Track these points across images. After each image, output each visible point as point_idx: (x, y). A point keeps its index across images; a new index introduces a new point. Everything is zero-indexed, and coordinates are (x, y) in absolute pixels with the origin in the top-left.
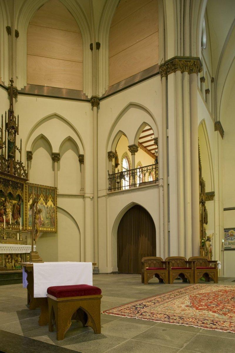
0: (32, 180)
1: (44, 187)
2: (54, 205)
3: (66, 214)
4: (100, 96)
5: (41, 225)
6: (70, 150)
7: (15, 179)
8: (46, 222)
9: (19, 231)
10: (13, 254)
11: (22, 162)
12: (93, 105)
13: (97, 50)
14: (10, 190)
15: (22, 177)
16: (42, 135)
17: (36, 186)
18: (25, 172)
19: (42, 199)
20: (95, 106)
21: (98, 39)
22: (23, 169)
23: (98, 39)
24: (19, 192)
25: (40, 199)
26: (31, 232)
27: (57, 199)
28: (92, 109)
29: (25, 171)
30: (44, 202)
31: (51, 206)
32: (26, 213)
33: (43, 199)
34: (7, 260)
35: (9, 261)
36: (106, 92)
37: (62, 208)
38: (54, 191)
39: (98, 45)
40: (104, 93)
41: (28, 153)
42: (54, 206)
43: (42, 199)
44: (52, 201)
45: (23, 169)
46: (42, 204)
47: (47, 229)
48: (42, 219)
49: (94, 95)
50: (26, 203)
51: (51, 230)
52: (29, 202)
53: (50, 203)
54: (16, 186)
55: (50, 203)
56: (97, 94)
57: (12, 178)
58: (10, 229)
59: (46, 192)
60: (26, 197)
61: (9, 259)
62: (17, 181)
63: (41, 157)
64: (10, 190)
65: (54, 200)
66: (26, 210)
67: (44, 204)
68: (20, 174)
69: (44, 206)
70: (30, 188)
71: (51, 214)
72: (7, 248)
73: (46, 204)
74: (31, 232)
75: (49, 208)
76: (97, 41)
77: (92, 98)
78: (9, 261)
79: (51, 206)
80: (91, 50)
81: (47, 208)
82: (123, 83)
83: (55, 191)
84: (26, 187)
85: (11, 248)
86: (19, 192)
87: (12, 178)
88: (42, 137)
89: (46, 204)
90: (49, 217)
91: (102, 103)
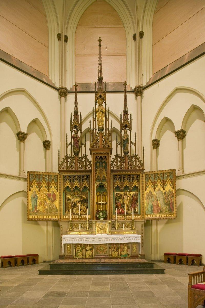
0: (148, 168)
1: (161, 172)
2: (173, 189)
3: (190, 195)
4: (144, 84)
5: (158, 212)
6: (168, 131)
7: (130, 172)
8: (164, 208)
9: (69, 221)
10: (119, 243)
11: (137, 154)
12: (137, 95)
13: (141, 39)
14: (126, 183)
15: (138, 168)
16: (165, 118)
17: (152, 173)
18: (140, 163)
19: (159, 185)
20: (139, 95)
21: (142, 28)
22: (139, 160)
23: (142, 28)
24: (135, 183)
25: (157, 185)
26: (157, 220)
27: (176, 181)
28: (136, 99)
29: (140, 162)
30: (161, 187)
31: (170, 190)
32: (143, 202)
33: (161, 185)
34: (113, 249)
35: (114, 250)
36: (150, 80)
37: (185, 189)
38: (173, 174)
39: (141, 35)
40: (148, 81)
41: (153, 142)
42: (173, 190)
43: (159, 185)
44: (170, 184)
45: (139, 160)
46: (159, 190)
47: (33, 217)
48: (160, 206)
49: (138, 85)
50: (143, 192)
51: (47, 217)
52: (146, 191)
53: (169, 187)
54: (131, 178)
55: (169, 187)
56: (141, 83)
57: (128, 172)
58: (124, 220)
59: (154, 177)
60: (143, 187)
61: (114, 248)
62: (133, 174)
63: (168, 140)
64: (126, 184)
65: (173, 184)
66: (143, 199)
67: (162, 190)
68: (136, 166)
69: (162, 192)
70: (146, 177)
71: (169, 199)
72: (114, 238)
73: (164, 189)
74: (157, 220)
75: (167, 193)
76: (140, 30)
77: (135, 88)
78: (114, 250)
79: (170, 190)
80: (134, 41)
81: (165, 193)
82: (187, 56)
83: (174, 173)
84: (142, 176)
85: (113, 238)
86: (135, 183)
87: (128, 172)
88: (167, 120)
89: (164, 189)
90: (167, 202)
91: (146, 92)
